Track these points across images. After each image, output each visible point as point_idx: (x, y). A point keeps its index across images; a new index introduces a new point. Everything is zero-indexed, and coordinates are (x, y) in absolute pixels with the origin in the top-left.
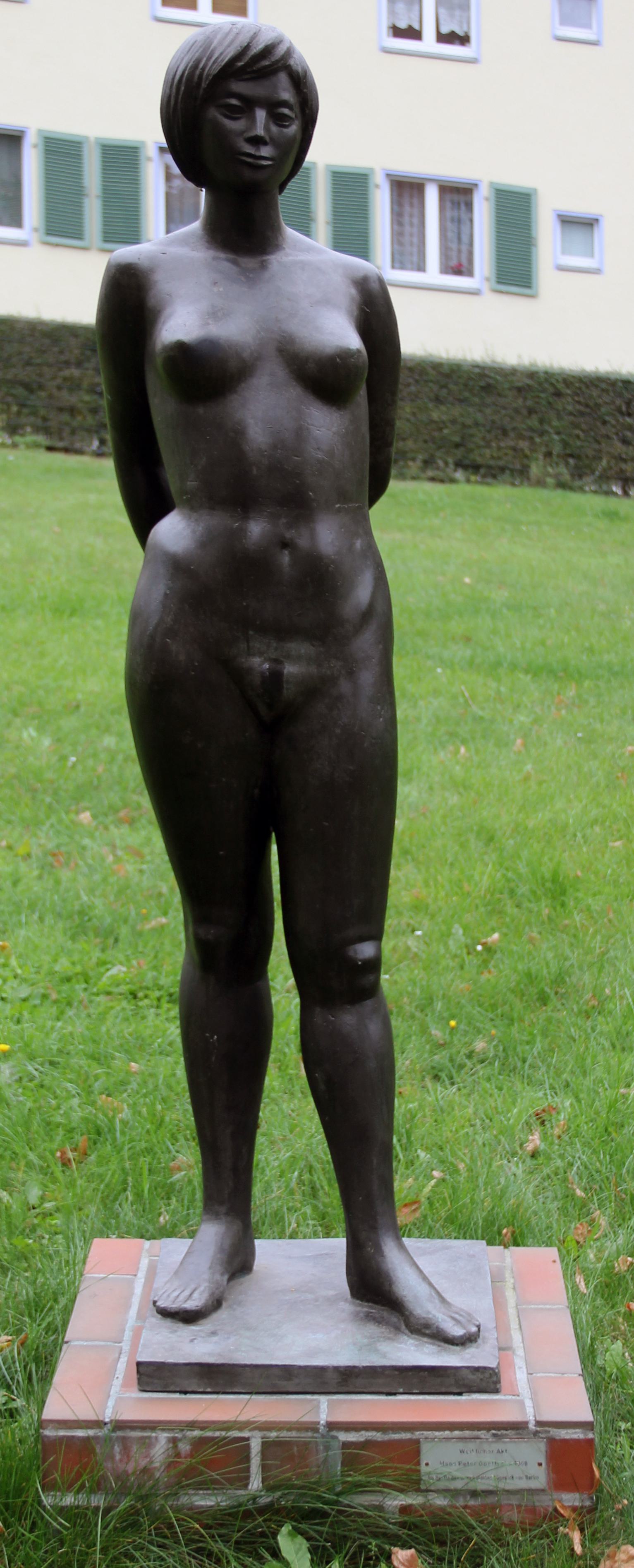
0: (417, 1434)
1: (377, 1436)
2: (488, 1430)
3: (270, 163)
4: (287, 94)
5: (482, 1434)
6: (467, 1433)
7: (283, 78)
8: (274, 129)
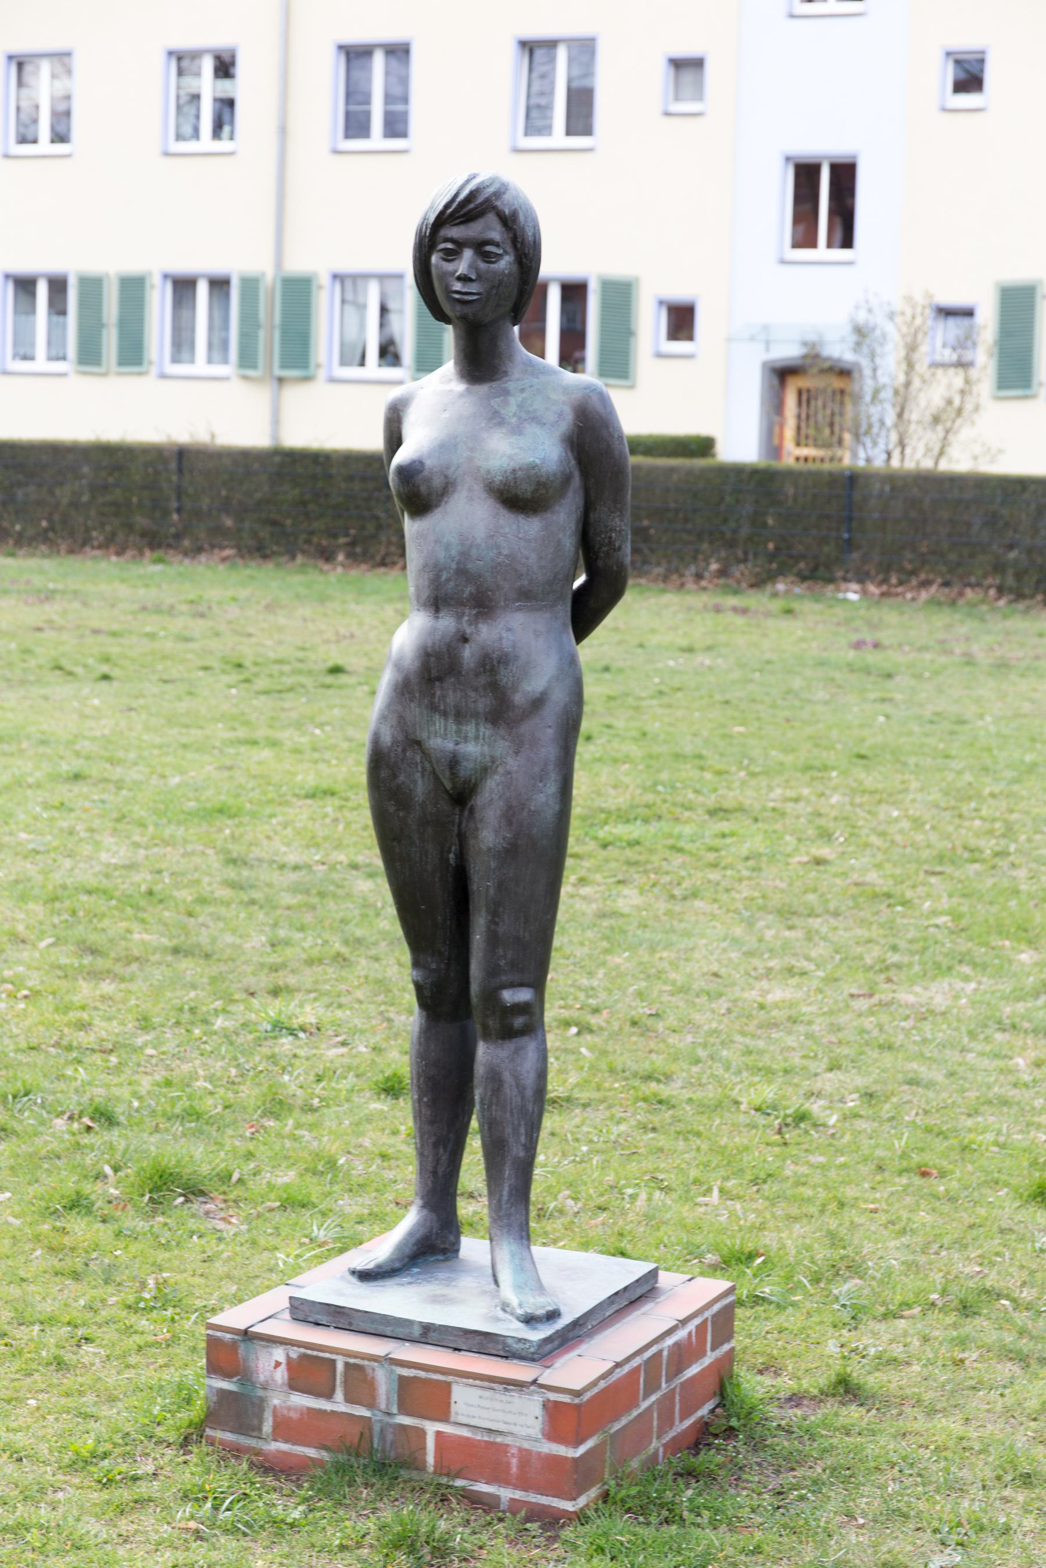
0: (450, 1378)
1: (422, 1374)
2: (501, 1383)
3: (475, 297)
4: (496, 233)
6: (486, 1384)
7: (491, 218)
8: (482, 265)
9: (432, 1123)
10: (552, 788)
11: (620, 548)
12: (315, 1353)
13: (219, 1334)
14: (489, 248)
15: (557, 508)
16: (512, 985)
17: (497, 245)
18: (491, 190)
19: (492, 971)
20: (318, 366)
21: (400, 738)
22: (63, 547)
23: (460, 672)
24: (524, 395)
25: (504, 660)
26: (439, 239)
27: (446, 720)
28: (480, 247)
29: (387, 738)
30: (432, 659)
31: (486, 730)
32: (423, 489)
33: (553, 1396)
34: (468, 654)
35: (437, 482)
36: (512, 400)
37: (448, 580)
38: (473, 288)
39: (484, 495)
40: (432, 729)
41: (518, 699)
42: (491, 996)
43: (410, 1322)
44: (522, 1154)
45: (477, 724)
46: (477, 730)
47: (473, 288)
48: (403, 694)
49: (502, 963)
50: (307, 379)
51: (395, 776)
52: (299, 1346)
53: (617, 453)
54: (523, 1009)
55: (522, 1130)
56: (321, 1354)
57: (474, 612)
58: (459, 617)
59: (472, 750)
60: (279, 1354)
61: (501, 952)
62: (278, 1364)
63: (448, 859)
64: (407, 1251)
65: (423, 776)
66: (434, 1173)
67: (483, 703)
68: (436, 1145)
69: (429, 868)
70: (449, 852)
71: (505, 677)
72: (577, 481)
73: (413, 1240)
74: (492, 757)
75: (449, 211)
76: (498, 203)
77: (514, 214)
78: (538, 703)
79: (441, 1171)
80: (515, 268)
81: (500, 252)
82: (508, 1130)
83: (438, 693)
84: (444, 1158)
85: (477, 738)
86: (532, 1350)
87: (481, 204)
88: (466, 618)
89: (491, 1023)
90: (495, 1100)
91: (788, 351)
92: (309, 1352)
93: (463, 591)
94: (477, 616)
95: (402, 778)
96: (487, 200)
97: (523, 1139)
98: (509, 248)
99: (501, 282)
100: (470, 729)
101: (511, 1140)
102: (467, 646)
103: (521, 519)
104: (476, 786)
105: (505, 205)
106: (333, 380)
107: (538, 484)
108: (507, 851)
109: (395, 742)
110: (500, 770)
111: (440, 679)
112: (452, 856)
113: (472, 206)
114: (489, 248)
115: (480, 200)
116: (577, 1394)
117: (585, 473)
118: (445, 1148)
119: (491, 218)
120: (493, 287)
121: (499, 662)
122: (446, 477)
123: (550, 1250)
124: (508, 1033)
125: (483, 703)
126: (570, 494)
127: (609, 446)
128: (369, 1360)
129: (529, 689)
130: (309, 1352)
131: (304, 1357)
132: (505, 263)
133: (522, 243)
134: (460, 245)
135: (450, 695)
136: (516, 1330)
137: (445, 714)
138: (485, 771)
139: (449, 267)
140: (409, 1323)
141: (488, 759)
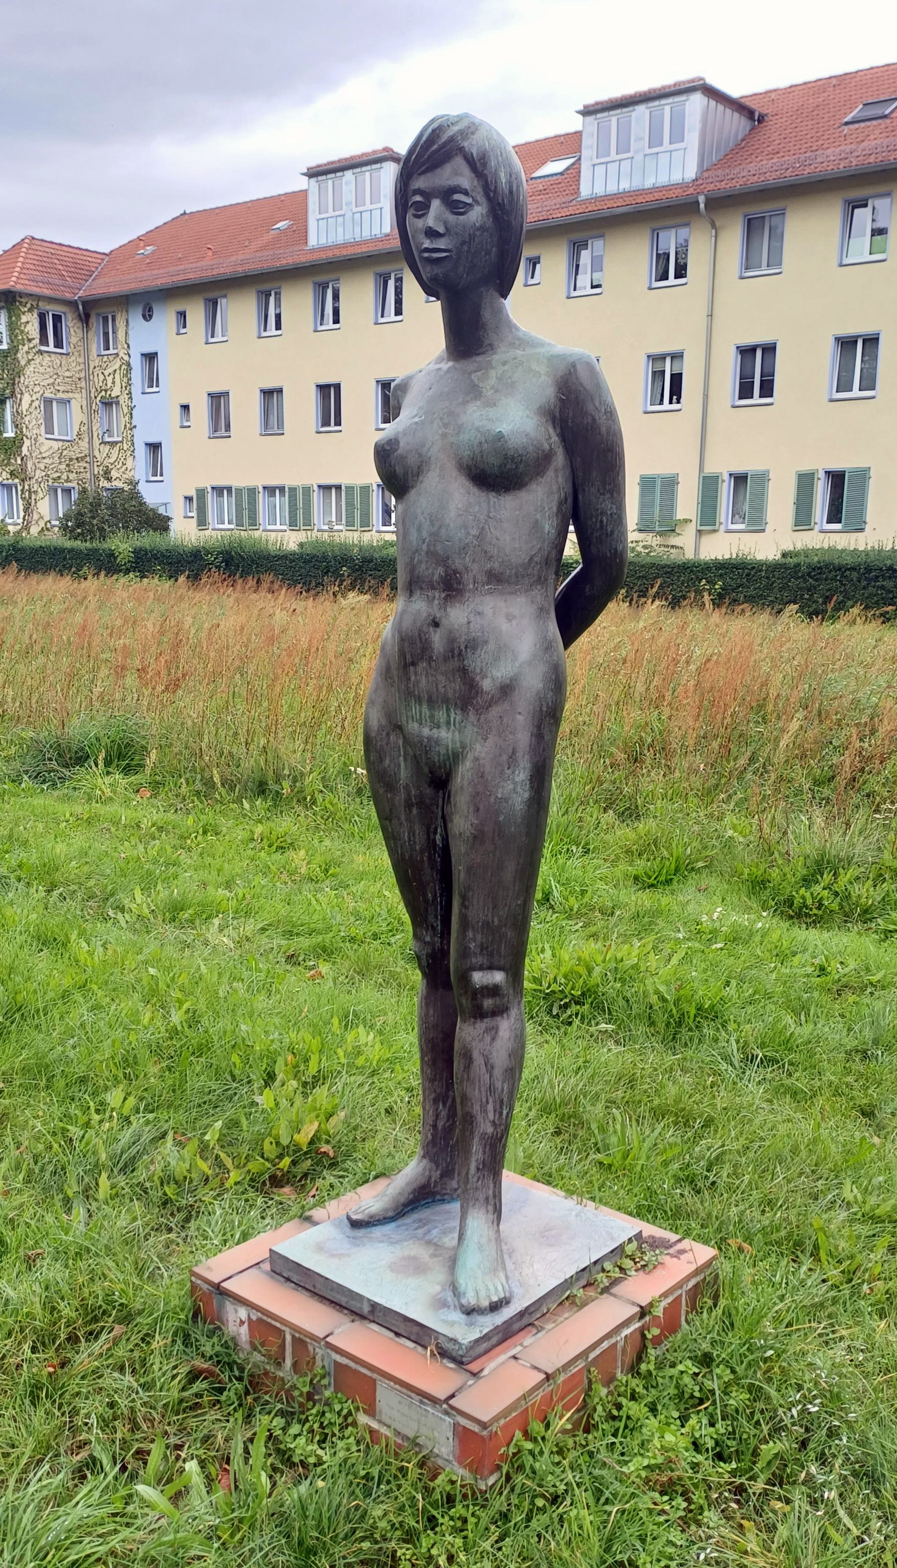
1: (352, 1364)
2: (418, 1394)
3: (444, 254)
4: (466, 180)
5: (413, 1395)
7: (459, 162)
8: (451, 218)
9: (432, 1081)
10: (522, 775)
11: (612, 532)
12: (269, 1320)
13: (199, 1282)
14: (457, 197)
15: (533, 486)
16: (481, 968)
17: (466, 193)
18: (455, 129)
19: (464, 953)
20: (721, 523)
21: (384, 722)
23: (431, 658)
24: (506, 368)
25: (473, 645)
26: (410, 193)
27: (421, 705)
28: (447, 195)
29: (374, 724)
30: (406, 644)
31: (456, 715)
32: (399, 470)
34: (437, 640)
35: (412, 461)
36: (493, 373)
37: (420, 562)
38: (441, 244)
39: (455, 473)
40: (409, 714)
41: (486, 684)
42: (465, 978)
44: (490, 1130)
45: (448, 710)
46: (449, 716)
47: (441, 244)
49: (472, 945)
50: (715, 531)
51: (381, 760)
52: (258, 1310)
53: (604, 430)
54: (493, 991)
55: (490, 1107)
56: (273, 1323)
57: (443, 595)
58: (430, 601)
59: (446, 736)
60: (243, 1313)
61: (470, 934)
62: (242, 1323)
63: (434, 840)
64: (402, 1200)
65: (405, 760)
66: (435, 1126)
67: (454, 687)
68: (435, 1101)
69: (417, 847)
70: (435, 833)
71: (474, 662)
72: (560, 459)
73: (410, 1189)
74: (461, 742)
76: (466, 144)
77: (484, 158)
78: (506, 690)
79: (440, 1125)
80: (489, 222)
81: (469, 200)
82: (477, 1108)
83: (413, 678)
84: (444, 1113)
85: (448, 723)
86: (461, 1352)
87: (445, 144)
88: (436, 602)
89: (464, 1001)
92: (265, 1318)
93: (433, 574)
94: (445, 599)
95: (387, 762)
96: (452, 139)
97: (491, 1116)
98: (480, 198)
99: (472, 237)
100: (441, 715)
101: (480, 1118)
102: (438, 630)
103: (492, 497)
105: (473, 145)
106: (728, 531)
107: (506, 457)
108: (475, 837)
109: (381, 728)
110: (470, 756)
111: (413, 664)
112: (438, 837)
113: (435, 147)
114: (457, 197)
115: (444, 138)
116: (484, 1425)
117: (570, 450)
118: (444, 1104)
119: (459, 162)
120: (464, 243)
121: (466, 647)
122: (420, 455)
123: (542, 1193)
124: (479, 1014)
125: (454, 687)
126: (550, 473)
127: (594, 420)
128: (311, 1339)
129: (499, 675)
131: (260, 1320)
132: (477, 214)
133: (495, 191)
134: (428, 196)
135: (422, 679)
136: (452, 1324)
137: (419, 700)
140: (359, 1297)
141: (458, 745)
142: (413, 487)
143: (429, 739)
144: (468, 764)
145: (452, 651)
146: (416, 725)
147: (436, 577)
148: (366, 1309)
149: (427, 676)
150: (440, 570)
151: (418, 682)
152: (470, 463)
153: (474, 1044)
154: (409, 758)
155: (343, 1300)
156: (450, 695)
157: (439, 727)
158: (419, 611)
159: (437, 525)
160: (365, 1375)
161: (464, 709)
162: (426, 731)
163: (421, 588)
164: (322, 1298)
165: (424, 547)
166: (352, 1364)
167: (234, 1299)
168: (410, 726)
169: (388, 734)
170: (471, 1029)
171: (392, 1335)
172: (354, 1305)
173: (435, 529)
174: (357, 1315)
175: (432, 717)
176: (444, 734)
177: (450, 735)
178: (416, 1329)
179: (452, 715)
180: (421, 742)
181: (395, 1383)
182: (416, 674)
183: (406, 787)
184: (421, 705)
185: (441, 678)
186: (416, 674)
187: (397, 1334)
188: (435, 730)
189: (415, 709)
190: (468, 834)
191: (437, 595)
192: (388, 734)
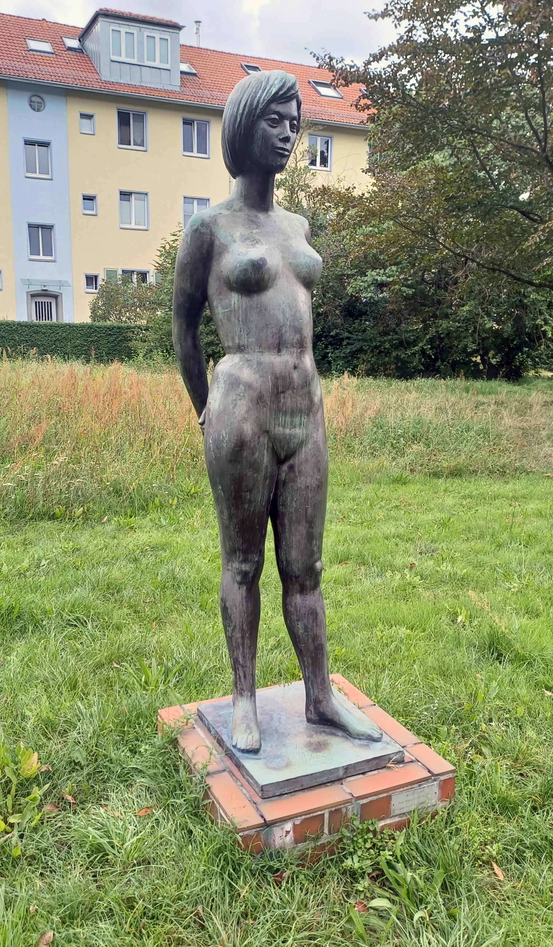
0: (390, 793)
1: (374, 798)
6: (410, 787)
12: (312, 815)
13: (246, 832)
21: (256, 430)
22: (250, 270)
23: (294, 387)
30: (280, 381)
33: (442, 778)
40: (277, 422)
43: (337, 769)
45: (301, 416)
46: (301, 420)
48: (258, 403)
51: (253, 454)
52: (297, 817)
57: (299, 351)
60: (289, 826)
75: (281, 93)
83: (282, 401)
90: (315, 625)
91: (37, 288)
100: (297, 420)
104: (295, 452)
109: (254, 434)
111: (283, 392)
130: (308, 816)
131: (303, 821)
137: (285, 413)
138: (302, 444)
139: (275, 131)
142: (270, 287)
143: (290, 435)
144: (310, 446)
145: (306, 382)
146: (281, 429)
147: (295, 340)
148: (341, 773)
149: (291, 398)
150: (298, 336)
151: (285, 402)
152: (307, 275)
153: (316, 604)
154: (269, 449)
155: (324, 779)
156: (303, 408)
157: (295, 427)
158: (287, 361)
159: (294, 310)
160: (377, 800)
161: (308, 415)
162: (287, 431)
163: (287, 347)
164: (324, 784)
165: (288, 323)
166: (374, 798)
167: (280, 821)
168: (276, 430)
169: (259, 437)
170: (312, 597)
171: (361, 776)
172: (333, 777)
173: (293, 313)
174: (340, 780)
175: (292, 422)
176: (298, 431)
177: (301, 431)
178: (375, 762)
179: (303, 419)
180: (285, 438)
181: (407, 786)
182: (284, 397)
183: (267, 467)
184: (285, 416)
185: (299, 399)
186: (284, 397)
187: (363, 773)
188: (293, 430)
189: (281, 419)
190: (314, 485)
191: (295, 351)
192: (259, 437)
